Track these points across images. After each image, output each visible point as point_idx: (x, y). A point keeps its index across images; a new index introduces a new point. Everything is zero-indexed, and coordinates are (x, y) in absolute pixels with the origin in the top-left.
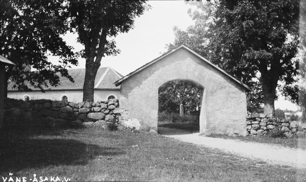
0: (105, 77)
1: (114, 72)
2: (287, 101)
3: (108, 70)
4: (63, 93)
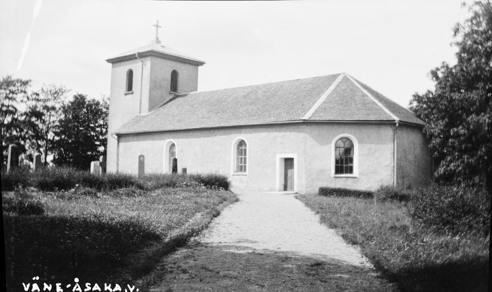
0: (332, 94)
1: (352, 83)
2: (439, 65)
3: (339, 79)
4: (238, 135)
